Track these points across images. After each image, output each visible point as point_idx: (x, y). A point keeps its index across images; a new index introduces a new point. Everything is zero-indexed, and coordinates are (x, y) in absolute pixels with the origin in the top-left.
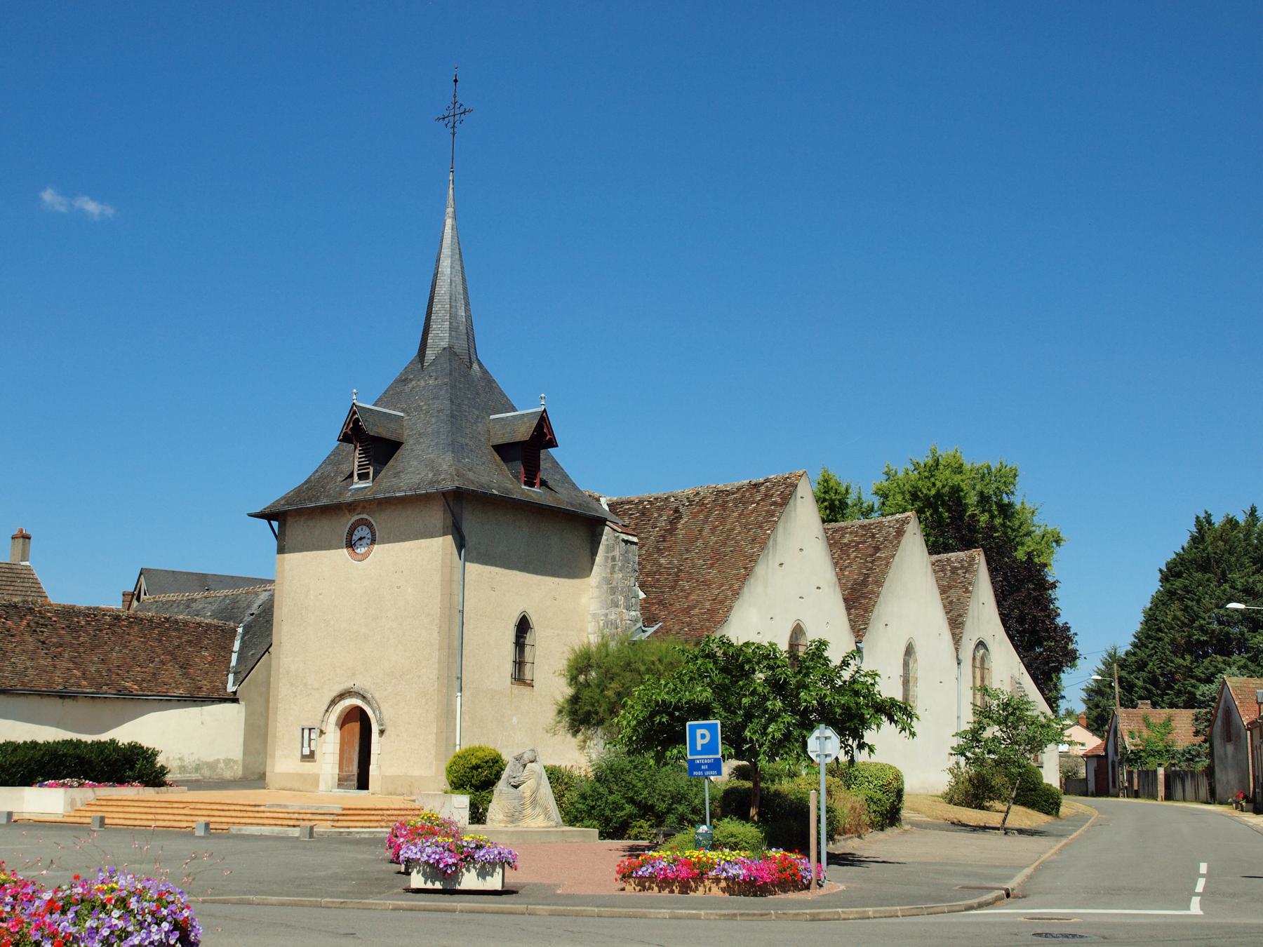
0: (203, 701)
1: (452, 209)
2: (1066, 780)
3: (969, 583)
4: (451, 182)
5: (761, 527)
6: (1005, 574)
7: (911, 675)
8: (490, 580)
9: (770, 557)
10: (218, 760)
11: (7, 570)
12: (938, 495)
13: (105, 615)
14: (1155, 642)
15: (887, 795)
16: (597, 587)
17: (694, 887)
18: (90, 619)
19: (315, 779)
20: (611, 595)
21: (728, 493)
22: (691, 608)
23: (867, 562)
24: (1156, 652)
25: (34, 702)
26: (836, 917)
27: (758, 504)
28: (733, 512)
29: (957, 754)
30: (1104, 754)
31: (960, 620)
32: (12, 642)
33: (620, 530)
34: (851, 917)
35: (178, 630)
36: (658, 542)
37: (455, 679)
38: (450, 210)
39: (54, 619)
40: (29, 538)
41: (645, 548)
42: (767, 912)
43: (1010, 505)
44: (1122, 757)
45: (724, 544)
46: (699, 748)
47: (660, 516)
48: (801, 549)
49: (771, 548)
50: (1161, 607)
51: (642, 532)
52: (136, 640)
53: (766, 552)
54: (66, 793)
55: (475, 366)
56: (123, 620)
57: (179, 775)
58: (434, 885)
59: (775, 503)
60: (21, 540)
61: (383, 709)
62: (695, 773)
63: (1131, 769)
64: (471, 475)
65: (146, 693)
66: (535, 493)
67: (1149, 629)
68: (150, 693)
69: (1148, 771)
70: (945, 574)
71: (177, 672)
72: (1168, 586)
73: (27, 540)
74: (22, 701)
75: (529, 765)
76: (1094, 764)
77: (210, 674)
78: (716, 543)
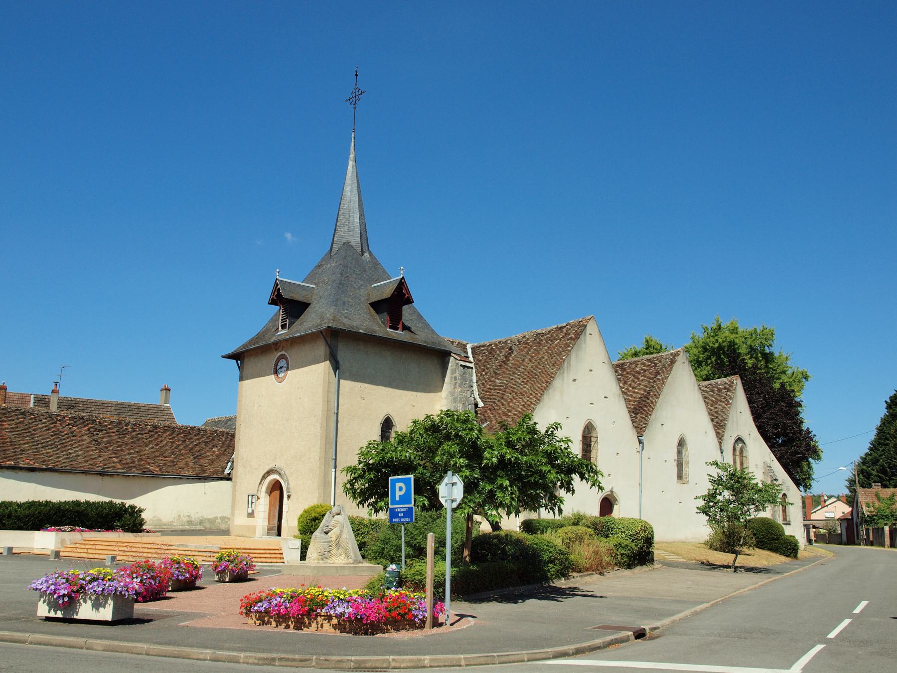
0: (205, 479)
1: (353, 155)
2: (829, 534)
3: (729, 398)
4: (353, 138)
5: (560, 355)
6: (765, 396)
7: (684, 460)
8: (360, 392)
9: (565, 374)
10: (216, 518)
11: (155, 409)
12: (720, 348)
13: (147, 425)
14: (883, 446)
15: (636, 542)
16: (446, 398)
17: (307, 623)
18: (135, 427)
19: (253, 529)
20: (454, 403)
21: (543, 334)
22: (509, 411)
23: (650, 383)
24: (885, 453)
25: (81, 478)
26: (384, 665)
27: (560, 340)
28: (545, 346)
29: (701, 512)
30: (851, 518)
31: (723, 423)
32: (73, 440)
33: (459, 359)
34: (402, 666)
35: (198, 435)
36: (496, 369)
37: (331, 459)
38: (352, 156)
39: (109, 426)
40: (170, 390)
41: (489, 374)
42: (308, 657)
43: (771, 354)
44: (862, 520)
45: (536, 368)
46: (397, 499)
47: (501, 353)
48: (591, 370)
49: (566, 368)
50: (887, 425)
51: (488, 364)
52: (166, 440)
53: (562, 371)
54: (57, 535)
55: (367, 255)
56: (160, 428)
57: (188, 527)
58: (56, 614)
59: (571, 339)
60: (165, 391)
61: (290, 481)
62: (394, 520)
63: (868, 527)
64: (345, 321)
65: (164, 473)
66: (399, 334)
67: (880, 438)
68: (166, 474)
69: (878, 528)
70: (714, 393)
71: (191, 461)
72: (891, 411)
73: (168, 391)
74: (71, 476)
75: (336, 516)
76: (845, 524)
77: (215, 462)
78: (532, 367)
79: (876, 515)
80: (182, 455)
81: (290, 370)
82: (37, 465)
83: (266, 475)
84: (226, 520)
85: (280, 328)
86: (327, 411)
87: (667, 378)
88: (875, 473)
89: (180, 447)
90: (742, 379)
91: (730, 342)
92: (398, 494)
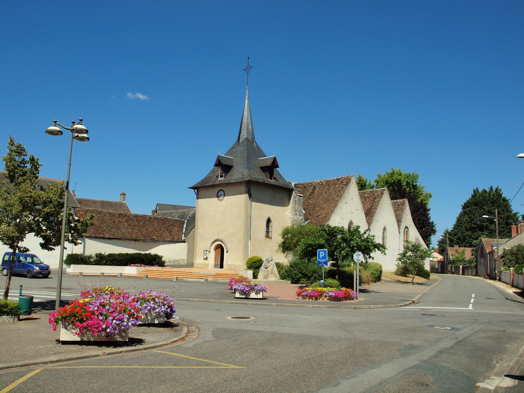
5: (340, 192)
12: (394, 182)
14: (460, 227)
16: (291, 209)
19: (208, 265)
21: (330, 181)
22: (319, 216)
24: (460, 230)
26: (361, 308)
33: (297, 192)
38: (247, 97)
39: (133, 218)
41: (305, 198)
43: (416, 185)
44: (449, 262)
45: (329, 197)
46: (321, 257)
47: (310, 188)
49: (343, 198)
55: (255, 143)
57: (169, 264)
60: (123, 195)
61: (227, 245)
65: (159, 240)
66: (272, 181)
68: (160, 240)
71: (168, 234)
72: (464, 210)
73: (125, 195)
76: (440, 264)
79: (456, 260)
80: (164, 231)
81: (226, 196)
82: (111, 237)
83: (214, 242)
84: (184, 260)
85: (219, 177)
86: (247, 215)
87: (380, 201)
88: (455, 240)
89: (162, 227)
90: (408, 200)
91: (398, 180)
92: (321, 256)
